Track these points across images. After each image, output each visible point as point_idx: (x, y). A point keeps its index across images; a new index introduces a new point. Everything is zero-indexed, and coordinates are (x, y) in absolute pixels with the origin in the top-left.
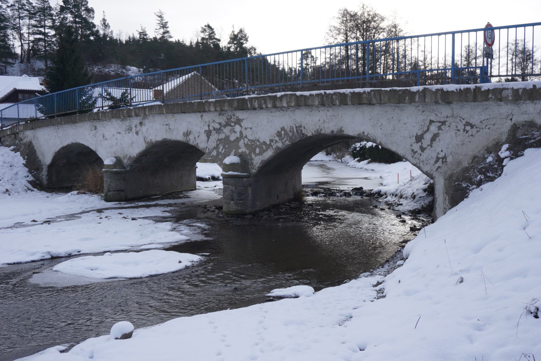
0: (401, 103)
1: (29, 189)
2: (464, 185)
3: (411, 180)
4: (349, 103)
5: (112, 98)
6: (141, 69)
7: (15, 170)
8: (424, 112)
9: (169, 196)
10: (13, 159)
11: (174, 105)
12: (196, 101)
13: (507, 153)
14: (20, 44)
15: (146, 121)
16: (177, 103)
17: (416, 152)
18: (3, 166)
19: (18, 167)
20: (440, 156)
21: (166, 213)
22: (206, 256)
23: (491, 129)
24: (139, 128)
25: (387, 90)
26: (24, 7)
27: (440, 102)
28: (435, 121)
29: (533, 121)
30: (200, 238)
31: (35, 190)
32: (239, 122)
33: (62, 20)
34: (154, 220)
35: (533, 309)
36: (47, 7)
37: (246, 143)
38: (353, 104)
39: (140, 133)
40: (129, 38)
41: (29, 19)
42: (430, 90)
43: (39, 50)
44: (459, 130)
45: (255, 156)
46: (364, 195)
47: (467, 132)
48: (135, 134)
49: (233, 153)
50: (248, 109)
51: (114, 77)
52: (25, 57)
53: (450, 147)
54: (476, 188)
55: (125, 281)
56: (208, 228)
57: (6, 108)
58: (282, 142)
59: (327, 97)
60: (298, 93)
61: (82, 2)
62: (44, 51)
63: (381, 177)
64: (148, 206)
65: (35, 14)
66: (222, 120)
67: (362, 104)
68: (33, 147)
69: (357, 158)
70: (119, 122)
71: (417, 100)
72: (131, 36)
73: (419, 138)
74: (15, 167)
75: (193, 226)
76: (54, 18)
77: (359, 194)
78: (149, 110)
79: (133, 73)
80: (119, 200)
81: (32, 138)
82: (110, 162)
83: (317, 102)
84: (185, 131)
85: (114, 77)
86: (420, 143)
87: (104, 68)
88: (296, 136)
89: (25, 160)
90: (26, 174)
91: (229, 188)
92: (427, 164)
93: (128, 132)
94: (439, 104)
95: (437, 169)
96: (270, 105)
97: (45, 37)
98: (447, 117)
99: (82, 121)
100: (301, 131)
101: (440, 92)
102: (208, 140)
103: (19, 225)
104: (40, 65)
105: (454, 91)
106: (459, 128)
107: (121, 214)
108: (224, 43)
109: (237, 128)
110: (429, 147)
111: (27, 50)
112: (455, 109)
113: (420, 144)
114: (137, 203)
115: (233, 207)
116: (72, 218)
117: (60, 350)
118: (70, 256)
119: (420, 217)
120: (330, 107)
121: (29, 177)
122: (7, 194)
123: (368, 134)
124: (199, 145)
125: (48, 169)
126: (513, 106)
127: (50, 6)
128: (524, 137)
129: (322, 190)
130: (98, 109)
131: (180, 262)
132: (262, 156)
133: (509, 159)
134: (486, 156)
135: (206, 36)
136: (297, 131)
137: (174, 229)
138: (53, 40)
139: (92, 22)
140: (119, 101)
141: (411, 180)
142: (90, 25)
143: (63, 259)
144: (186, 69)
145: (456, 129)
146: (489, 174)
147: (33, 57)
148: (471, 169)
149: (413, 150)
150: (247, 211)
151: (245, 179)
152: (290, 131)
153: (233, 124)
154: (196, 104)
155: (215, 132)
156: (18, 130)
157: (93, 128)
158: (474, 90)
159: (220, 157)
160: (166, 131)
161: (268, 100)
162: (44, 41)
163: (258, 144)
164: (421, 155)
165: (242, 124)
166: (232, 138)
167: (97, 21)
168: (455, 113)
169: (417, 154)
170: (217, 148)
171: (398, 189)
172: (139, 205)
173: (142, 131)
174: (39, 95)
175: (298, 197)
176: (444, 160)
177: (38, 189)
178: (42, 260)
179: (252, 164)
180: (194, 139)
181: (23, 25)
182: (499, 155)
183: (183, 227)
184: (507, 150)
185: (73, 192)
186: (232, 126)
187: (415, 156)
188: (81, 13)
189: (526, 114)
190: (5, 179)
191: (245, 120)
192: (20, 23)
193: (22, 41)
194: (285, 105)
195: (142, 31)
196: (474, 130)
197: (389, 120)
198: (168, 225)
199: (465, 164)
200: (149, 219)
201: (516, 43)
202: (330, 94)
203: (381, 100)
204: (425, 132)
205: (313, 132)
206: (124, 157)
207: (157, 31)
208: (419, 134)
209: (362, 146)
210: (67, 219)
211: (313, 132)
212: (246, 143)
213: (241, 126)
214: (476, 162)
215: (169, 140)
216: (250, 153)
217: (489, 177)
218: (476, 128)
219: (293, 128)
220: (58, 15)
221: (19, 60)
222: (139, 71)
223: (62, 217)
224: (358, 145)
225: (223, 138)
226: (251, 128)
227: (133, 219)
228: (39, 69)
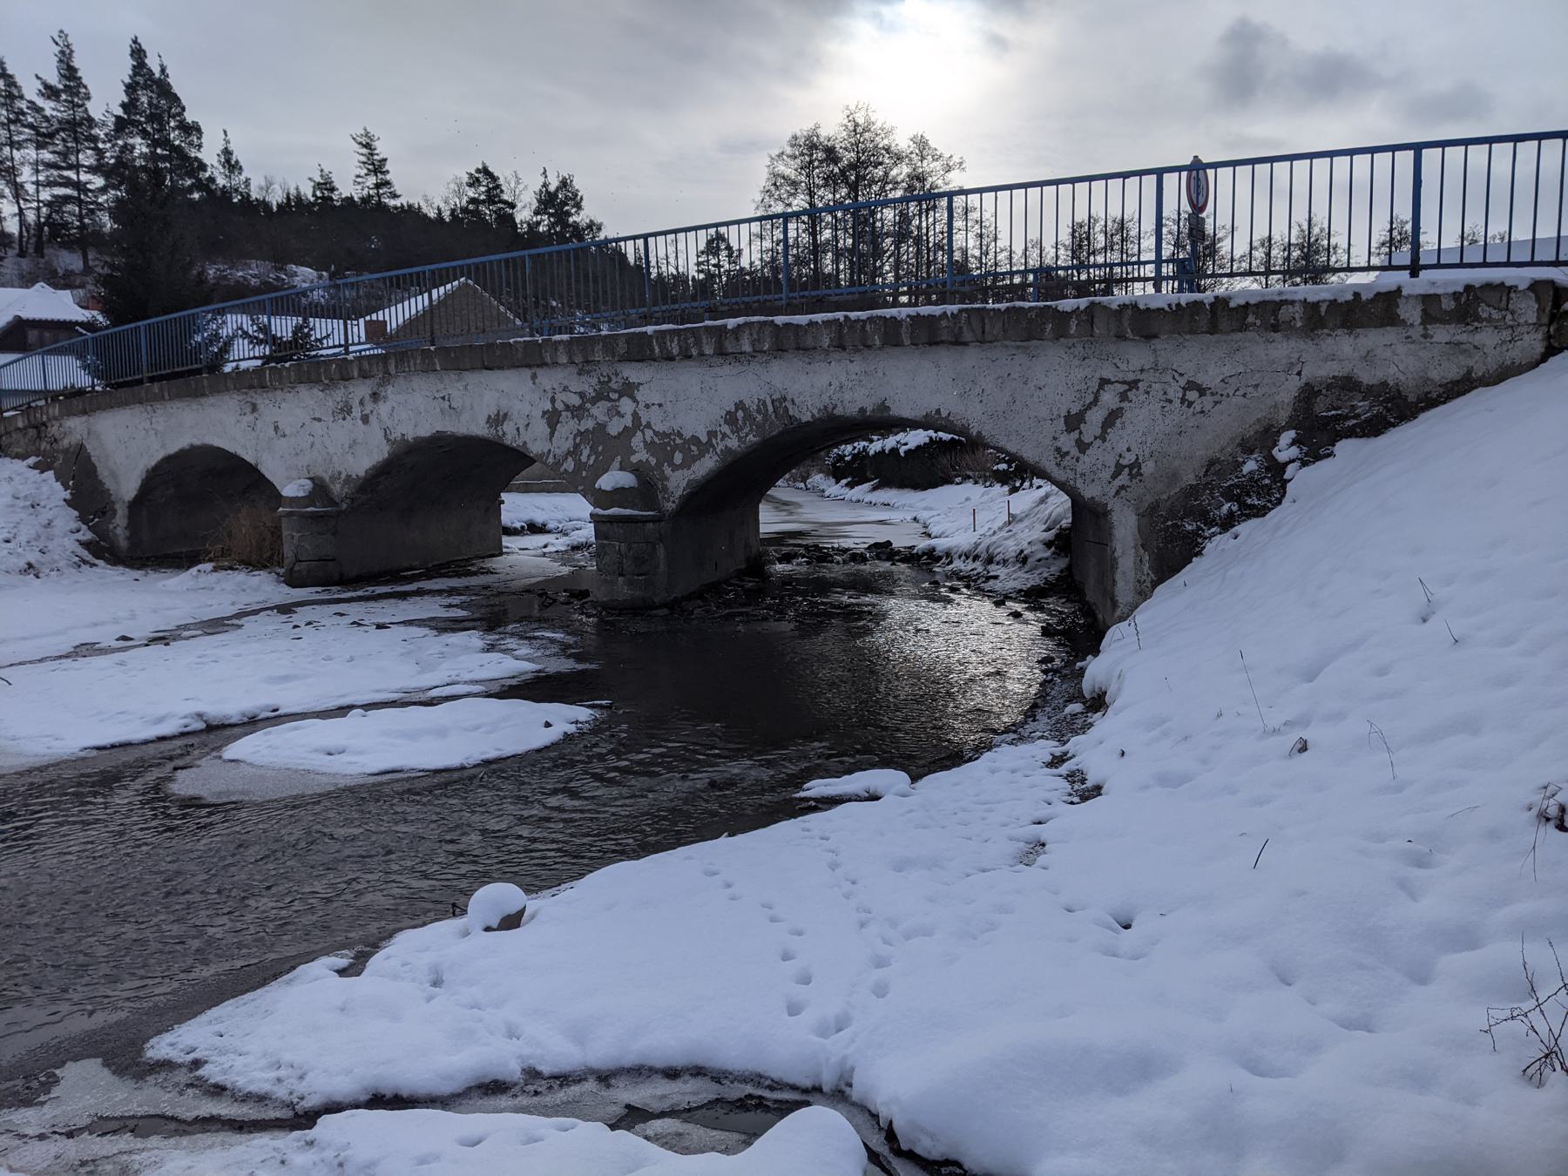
0: (1034, 339)
1: (85, 562)
2: (1189, 528)
3: (1010, 523)
4: (907, 342)
5: (274, 340)
6: (324, 273)
7: (45, 516)
8: (1087, 360)
9: (443, 571)
10: (37, 489)
11: (462, 348)
12: (519, 339)
13: (1294, 452)
14: (16, 210)
15: (390, 389)
16: (471, 346)
17: (1067, 453)
18: (13, 506)
19: (51, 509)
20: (1124, 462)
21: (455, 609)
22: (601, 707)
23: (1248, 396)
24: (369, 407)
25: (999, 310)
26: (21, 117)
27: (1130, 335)
28: (1113, 380)
29: (1351, 378)
30: (565, 665)
31: (100, 562)
32: (629, 390)
33: (122, 152)
34: (432, 628)
35: (1553, 811)
36: (83, 118)
37: (648, 439)
38: (915, 345)
39: (373, 419)
40: (288, 198)
41: (37, 148)
42: (1105, 308)
43: (65, 225)
44: (1170, 401)
45: (673, 471)
46: (897, 558)
47: (1190, 404)
48: (360, 422)
49: (616, 464)
50: (655, 360)
51: (257, 291)
52: (31, 241)
54: (1220, 533)
55: (424, 779)
56: (576, 642)
57: (12, 363)
59: (849, 328)
60: (780, 320)
61: (171, 108)
62: (78, 227)
63: (915, 519)
64: (403, 596)
65: (51, 135)
66: (588, 385)
67: (937, 343)
68: (89, 457)
69: (845, 478)
71: (1072, 332)
72: (293, 192)
73: (1073, 422)
74: (45, 507)
75: (535, 638)
76: (101, 145)
77: (884, 557)
78: (397, 362)
79: (304, 282)
80: (326, 582)
81: (85, 437)
82: (298, 490)
83: (828, 340)
84: (493, 412)
85: (257, 291)
86: (1077, 431)
87: (231, 268)
88: (772, 423)
89: (69, 491)
90: (74, 525)
91: (614, 546)
93: (341, 416)
94: (1126, 339)
95: (1117, 493)
96: (708, 350)
97: (79, 194)
98: (1142, 370)
99: (219, 392)
100: (786, 409)
101: (1129, 312)
102: (552, 434)
104: (70, 261)
105: (1163, 309)
106: (1171, 395)
107: (342, 615)
109: (626, 405)
111: (36, 224)
113: (1075, 435)
115: (623, 591)
116: (220, 629)
117: (336, 968)
118: (252, 723)
119: (1049, 604)
120: (857, 350)
121: (81, 532)
122: (32, 575)
123: (949, 414)
125: (129, 511)
126: (1302, 342)
127: (90, 116)
128: (1333, 412)
129: (802, 551)
130: (234, 364)
131: (548, 725)
133: (1297, 464)
134: (1241, 460)
135: (480, 195)
136: (774, 411)
137: (491, 648)
138: (100, 200)
139: (196, 158)
140: (288, 345)
141: (1010, 523)
142: (192, 164)
143: (236, 730)
144: (454, 268)
145: (1163, 398)
146: (1253, 501)
147: (49, 241)
148: (1204, 490)
149: (1058, 450)
151: (650, 525)
152: (759, 411)
153: (614, 396)
154: (518, 346)
155: (569, 414)
156: (45, 417)
157: (248, 410)
158: (1212, 305)
159: (584, 474)
160: (442, 411)
161: (704, 337)
162: (80, 202)
163: (678, 441)
164: (1077, 461)
166: (615, 428)
167: (209, 154)
168: (1161, 361)
169: (1068, 458)
170: (574, 452)
171: (979, 544)
173: (379, 414)
174: (84, 332)
175: (756, 567)
176: (1135, 470)
177: (108, 561)
178: (183, 735)
179: (665, 489)
180: (515, 432)
181: (22, 164)
182: (1272, 456)
183: (512, 640)
184: (1292, 444)
185: (200, 567)
186: (614, 401)
187: (1064, 463)
188: (169, 135)
189: (1333, 360)
190: (23, 538)
191: (646, 386)
192: (12, 159)
193: (21, 202)
194: (747, 348)
195: (322, 181)
196: (1208, 400)
197: (1000, 380)
198: (474, 639)
199: (1189, 479)
200: (419, 626)
202: (858, 321)
203: (983, 332)
204: (1089, 407)
205: (815, 412)
207: (359, 180)
209: (856, 451)
210: (208, 631)
211: (815, 412)
212: (648, 439)
213: (635, 400)
214: (1216, 473)
215: (450, 436)
216: (659, 465)
217: (1252, 507)
218: (1212, 394)
219: (765, 402)
220: (110, 138)
221: (14, 248)
222: (320, 277)
223: (192, 627)
224: (847, 449)
225: (591, 429)
226: (660, 405)
227: (380, 626)
228: (66, 270)
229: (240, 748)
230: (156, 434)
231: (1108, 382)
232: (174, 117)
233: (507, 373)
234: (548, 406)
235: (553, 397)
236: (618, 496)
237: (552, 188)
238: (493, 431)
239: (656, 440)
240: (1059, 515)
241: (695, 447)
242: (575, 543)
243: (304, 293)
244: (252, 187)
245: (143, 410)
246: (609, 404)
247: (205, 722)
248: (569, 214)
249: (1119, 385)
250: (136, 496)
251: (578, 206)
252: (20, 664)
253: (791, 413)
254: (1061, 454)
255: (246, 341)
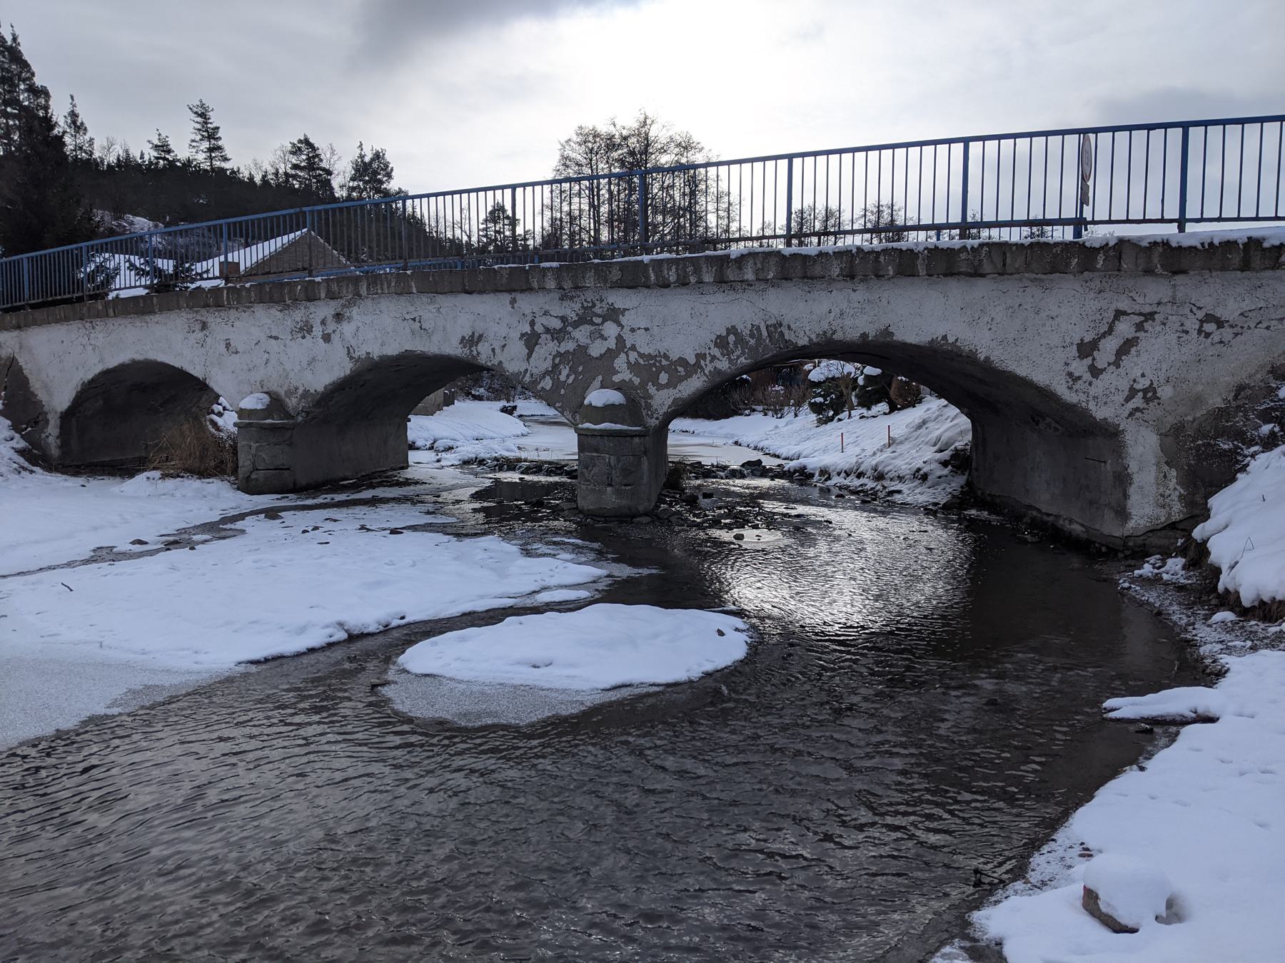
4: (922, 272)
17: (1079, 378)
24: (331, 326)
28: (1129, 311)
32: (614, 315)
37: (632, 360)
39: (335, 338)
44: (1187, 332)
45: (657, 390)
47: (1208, 335)
50: (648, 287)
53: (1164, 367)
54: (1263, 452)
58: (729, 359)
66: (571, 310)
67: (952, 274)
68: (21, 369)
70: (275, 312)
71: (1099, 266)
73: (1086, 349)
77: (759, 473)
81: (17, 350)
84: (467, 333)
86: (1090, 358)
88: (766, 346)
90: (8, 433)
91: (604, 458)
92: (1106, 403)
93: (300, 335)
95: (1131, 414)
96: (708, 278)
98: (1159, 304)
100: (782, 334)
101: (1160, 249)
102: (530, 355)
103: (105, 555)
105: (1195, 248)
106: (1188, 326)
108: (341, 181)
109: (610, 329)
110: (1112, 368)
112: (1182, 288)
113: (1089, 361)
114: (329, 496)
120: (865, 279)
121: (15, 441)
123: (957, 340)
124: (505, 365)
130: (116, 292)
132: (677, 391)
134: (1274, 385)
149: (1070, 374)
150: (641, 508)
151: (637, 440)
152: (752, 336)
154: (504, 272)
155: (549, 337)
157: (198, 326)
158: (1244, 245)
159: (563, 392)
163: (664, 362)
164: (1090, 384)
165: (624, 320)
166: (596, 349)
168: (1179, 295)
169: (1080, 382)
170: (553, 371)
172: (337, 500)
173: (342, 333)
179: (649, 407)
191: (632, 312)
194: (750, 276)
196: (1227, 333)
197: (1011, 310)
199: (1218, 402)
201: (879, 211)
203: (1004, 265)
204: (1104, 335)
205: (813, 336)
206: (289, 393)
207: (194, 144)
208: (1086, 340)
212: (632, 360)
216: (643, 385)
219: (758, 327)
222: (156, 226)
225: (571, 350)
229: (419, 658)
230: (94, 350)
231: (1125, 313)
232: (24, 80)
233: (485, 297)
234: (527, 329)
235: (533, 321)
236: (608, 412)
237: (367, 159)
238: (467, 351)
239: (641, 361)
240: (950, 438)
241: (686, 368)
242: (466, 458)
243: (141, 238)
244: (95, 146)
245: (80, 326)
246: (593, 328)
247: (346, 631)
248: (381, 182)
249: (1136, 317)
250: (69, 407)
251: (389, 176)
252: (50, 568)
253: (787, 337)
254: (1075, 379)
255: (133, 273)
